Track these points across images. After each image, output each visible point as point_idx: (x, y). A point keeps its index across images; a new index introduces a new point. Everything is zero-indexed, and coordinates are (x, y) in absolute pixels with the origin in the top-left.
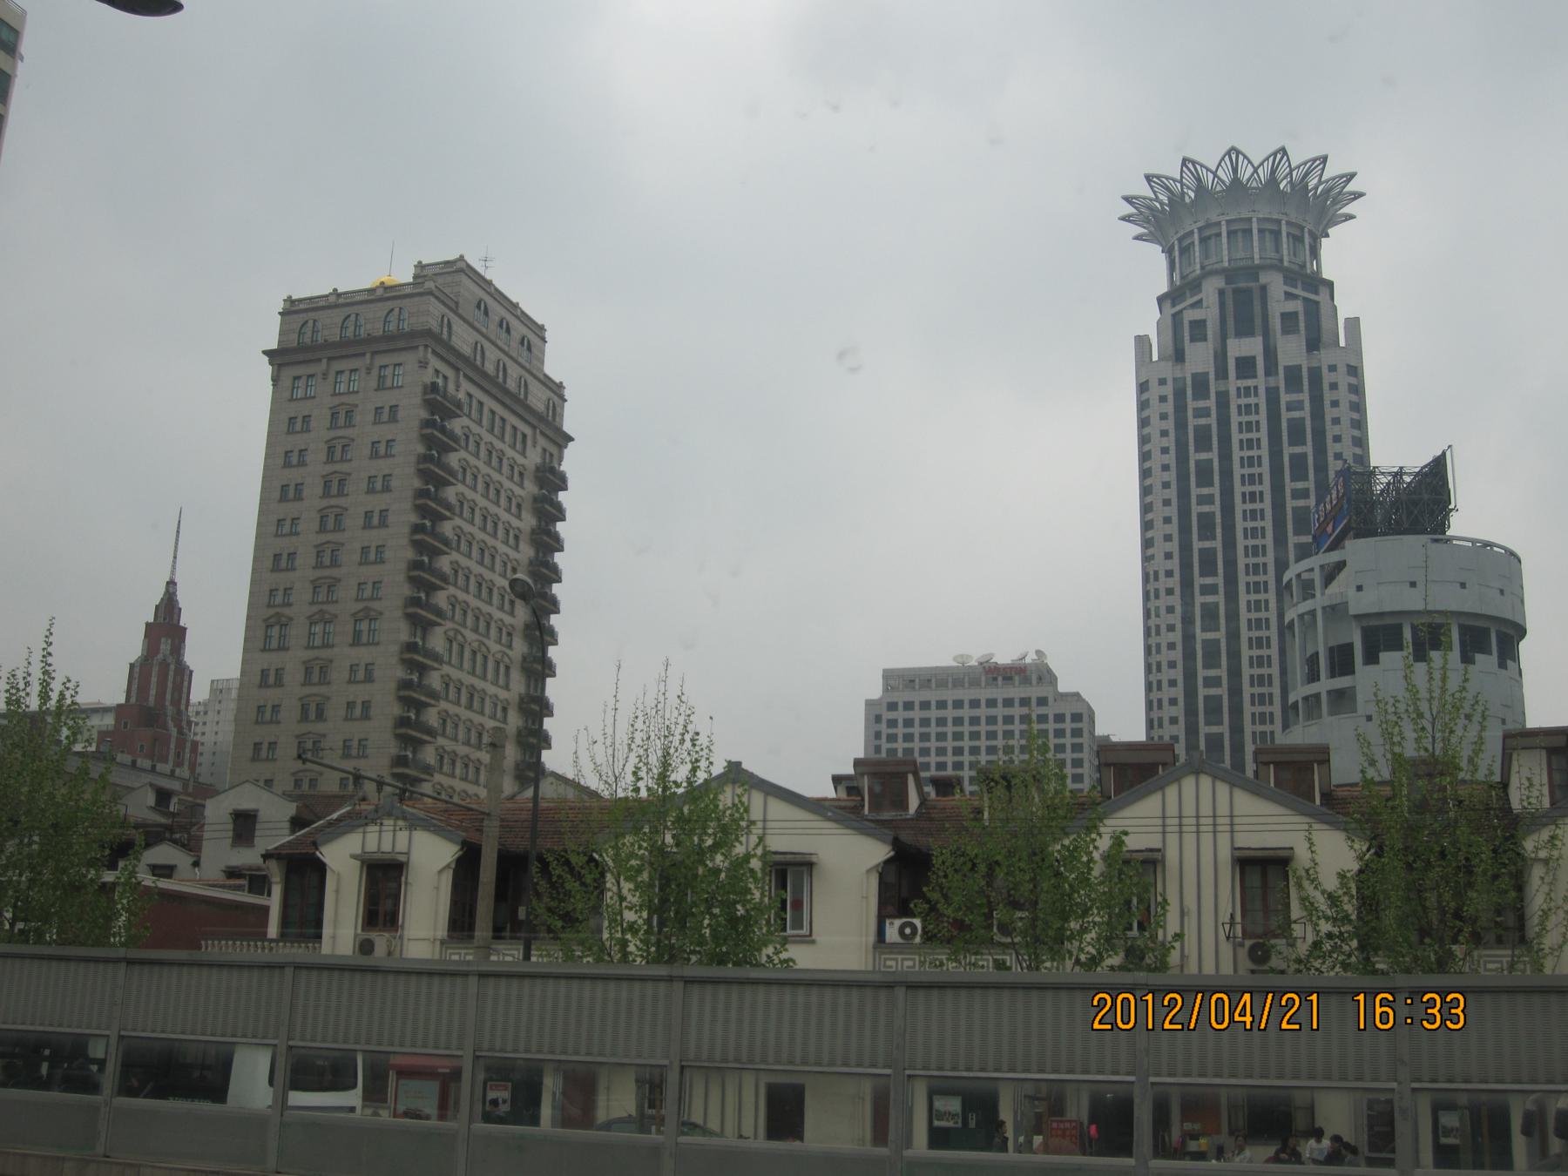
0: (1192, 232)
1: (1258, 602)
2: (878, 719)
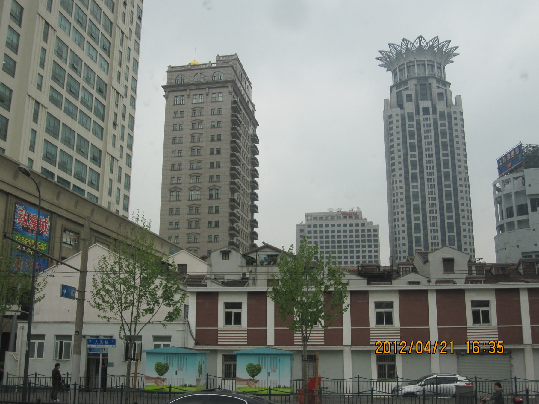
0: (404, 64)
1: (432, 191)
2: (302, 231)
